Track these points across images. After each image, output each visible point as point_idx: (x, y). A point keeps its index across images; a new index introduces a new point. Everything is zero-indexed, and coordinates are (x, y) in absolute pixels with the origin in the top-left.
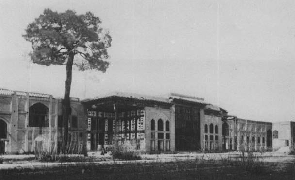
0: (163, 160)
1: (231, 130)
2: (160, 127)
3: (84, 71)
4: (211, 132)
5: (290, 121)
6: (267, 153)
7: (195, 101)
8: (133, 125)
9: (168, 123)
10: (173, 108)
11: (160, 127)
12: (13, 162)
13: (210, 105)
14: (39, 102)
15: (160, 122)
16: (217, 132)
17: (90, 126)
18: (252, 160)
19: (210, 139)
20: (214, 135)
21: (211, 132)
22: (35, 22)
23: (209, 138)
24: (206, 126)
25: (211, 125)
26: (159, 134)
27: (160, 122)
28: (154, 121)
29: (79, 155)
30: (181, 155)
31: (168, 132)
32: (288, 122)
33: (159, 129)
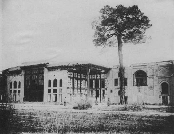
0: (170, 113)
3: (143, 39)
4: (15, 87)
5: (2, 71)
9: (20, 83)
10: (23, 73)
11: (55, 85)
13: (10, 69)
14: (139, 69)
15: (55, 81)
16: (19, 87)
19: (14, 93)
20: (17, 89)
21: (15, 87)
22: (138, 9)
24: (50, 81)
25: (15, 83)
26: (14, 90)
28: (16, 82)
33: (54, 86)
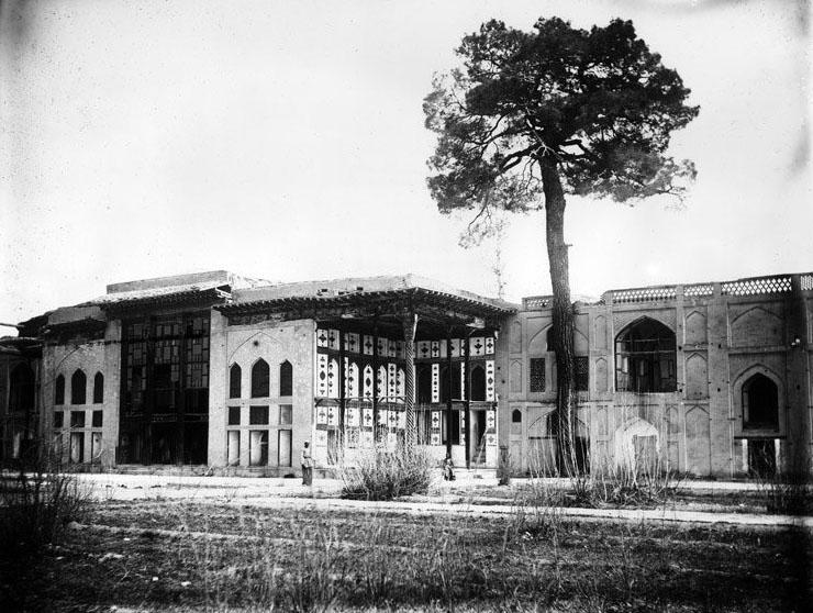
1: (435, 383)
2: (260, 388)
6: (273, 507)
7: (137, 294)
8: (351, 379)
10: (114, 332)
11: (260, 388)
12: (456, 514)
15: (261, 369)
16: (98, 398)
17: (488, 376)
18: (58, 484)
21: (79, 398)
23: (245, 415)
24: (235, 372)
27: (261, 369)
29: (550, 510)
30: (177, 480)
31: (235, 402)
32: (503, 267)
33: (254, 395)
